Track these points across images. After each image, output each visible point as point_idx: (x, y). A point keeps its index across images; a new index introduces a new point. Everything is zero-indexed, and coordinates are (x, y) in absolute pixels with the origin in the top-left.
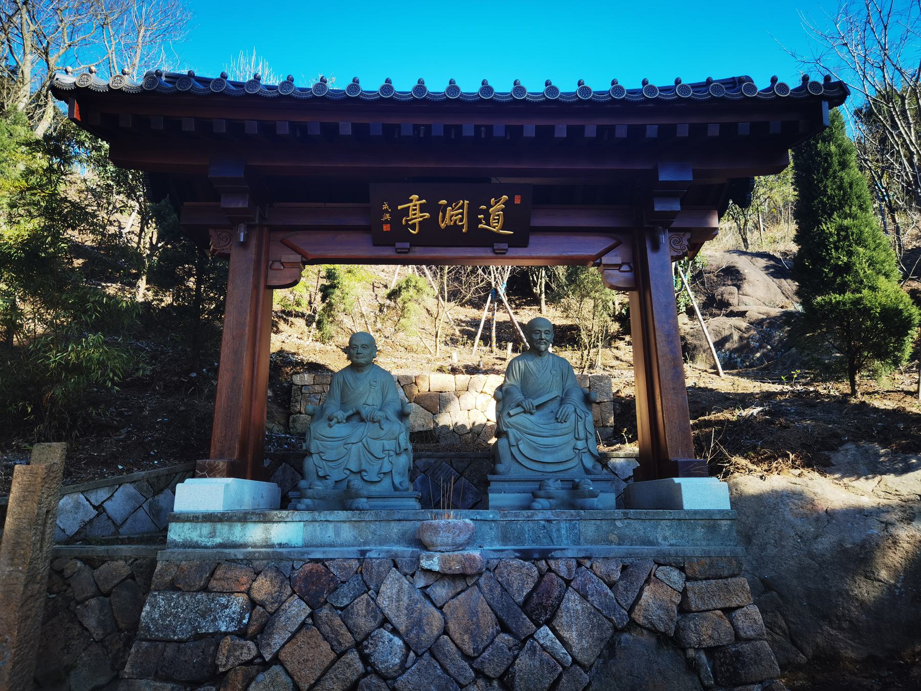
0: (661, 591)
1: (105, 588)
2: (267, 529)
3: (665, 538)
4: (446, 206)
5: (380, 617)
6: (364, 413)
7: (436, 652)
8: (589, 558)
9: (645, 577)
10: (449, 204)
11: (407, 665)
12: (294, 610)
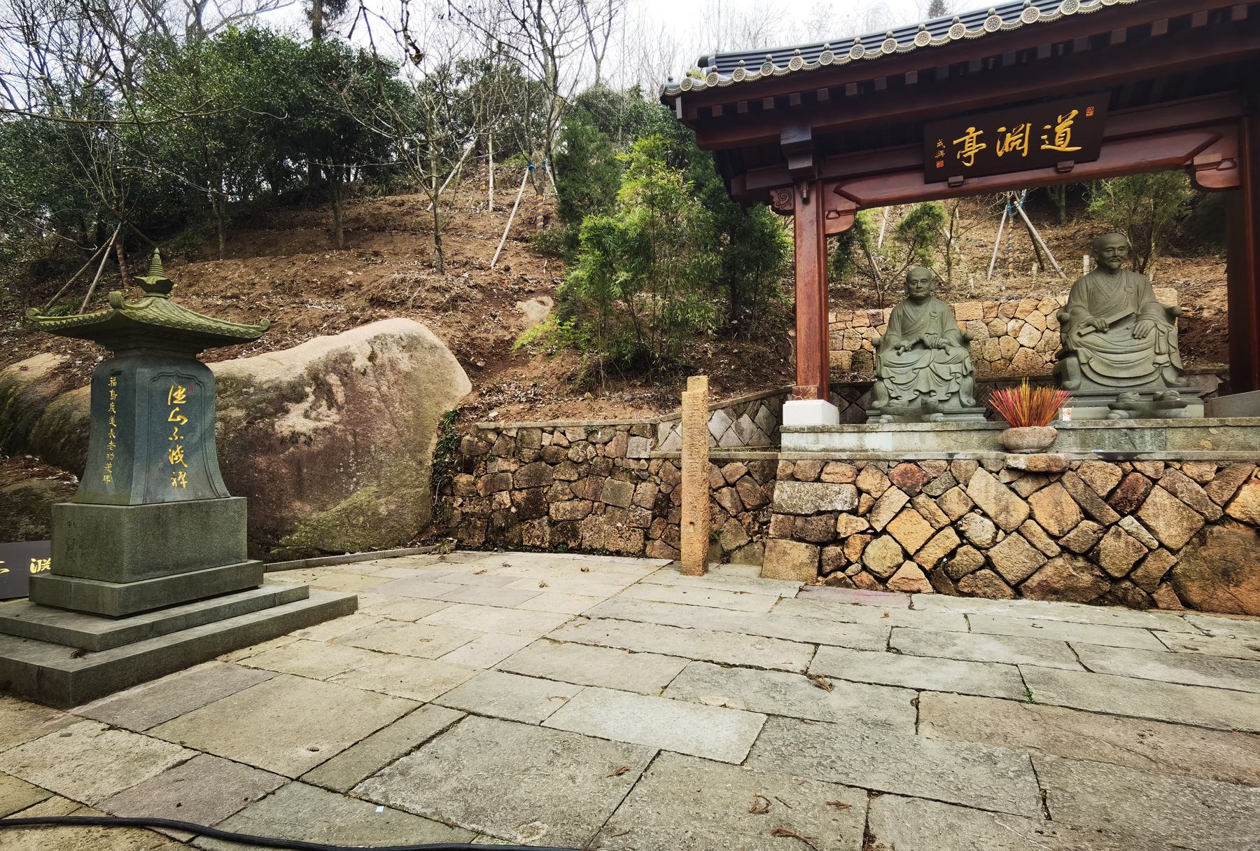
1: (731, 480)
4: (1004, 134)
5: (971, 504)
6: (928, 340)
7: (1023, 531)
8: (1179, 461)
9: (1244, 477)
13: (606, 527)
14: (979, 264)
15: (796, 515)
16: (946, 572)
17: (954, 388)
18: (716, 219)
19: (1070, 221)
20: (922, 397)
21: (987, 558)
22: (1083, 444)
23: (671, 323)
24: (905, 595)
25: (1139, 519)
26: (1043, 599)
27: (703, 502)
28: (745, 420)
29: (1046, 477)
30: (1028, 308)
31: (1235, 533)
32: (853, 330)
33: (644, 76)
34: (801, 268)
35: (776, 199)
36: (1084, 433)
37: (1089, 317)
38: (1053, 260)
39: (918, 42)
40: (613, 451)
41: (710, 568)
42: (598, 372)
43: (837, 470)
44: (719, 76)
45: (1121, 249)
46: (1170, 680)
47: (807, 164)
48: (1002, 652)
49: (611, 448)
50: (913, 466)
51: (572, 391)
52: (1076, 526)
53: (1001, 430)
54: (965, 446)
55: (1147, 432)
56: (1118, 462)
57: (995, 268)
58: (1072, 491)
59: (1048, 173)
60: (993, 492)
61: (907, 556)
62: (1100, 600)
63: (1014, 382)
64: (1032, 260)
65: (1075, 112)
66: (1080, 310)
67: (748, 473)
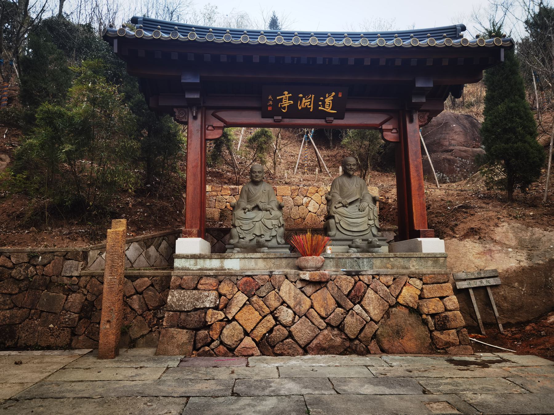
0: (411, 289)
1: (140, 290)
2: (222, 262)
3: (413, 266)
4: (302, 98)
5: (281, 300)
6: (261, 205)
7: (308, 315)
8: (378, 275)
10: (304, 97)
11: (295, 321)
12: (241, 298)
13: (39, 328)
14: (290, 166)
15: (181, 312)
16: (268, 342)
17: (274, 234)
18: (138, 120)
19: (334, 148)
20: (257, 238)
21: (290, 332)
22: (337, 266)
23: (103, 182)
24: (244, 358)
25: (362, 306)
26: (318, 354)
27: (117, 306)
28: (152, 250)
29: (319, 284)
30: (313, 191)
31: (401, 311)
32: (220, 196)
33: (95, 18)
34: (191, 157)
35: (177, 114)
36: (337, 260)
37: (340, 199)
38: (326, 167)
39: (260, 40)
40: (50, 271)
41: (120, 352)
42: (43, 213)
43: (207, 282)
44: (144, 32)
45: (354, 165)
46: (374, 393)
47: (197, 96)
48: (291, 387)
49: (49, 269)
50: (250, 279)
51: (20, 226)
52: (334, 311)
53: (297, 258)
54: (279, 267)
55: (365, 260)
56: (352, 276)
57: (298, 168)
58: (332, 292)
59: (321, 122)
60: (293, 294)
61: (246, 334)
62: (345, 351)
63: (303, 231)
64: (316, 166)
65: (333, 94)
66: (336, 195)
67: (152, 285)
